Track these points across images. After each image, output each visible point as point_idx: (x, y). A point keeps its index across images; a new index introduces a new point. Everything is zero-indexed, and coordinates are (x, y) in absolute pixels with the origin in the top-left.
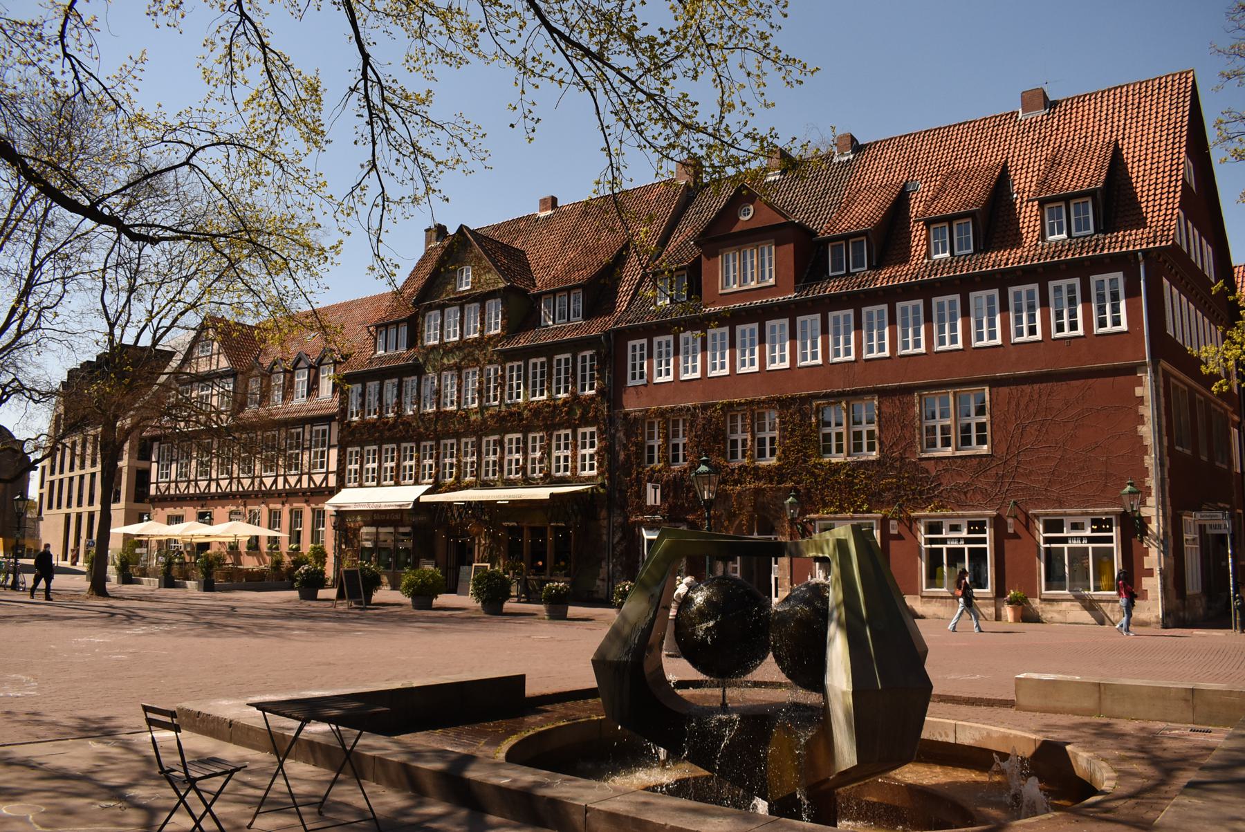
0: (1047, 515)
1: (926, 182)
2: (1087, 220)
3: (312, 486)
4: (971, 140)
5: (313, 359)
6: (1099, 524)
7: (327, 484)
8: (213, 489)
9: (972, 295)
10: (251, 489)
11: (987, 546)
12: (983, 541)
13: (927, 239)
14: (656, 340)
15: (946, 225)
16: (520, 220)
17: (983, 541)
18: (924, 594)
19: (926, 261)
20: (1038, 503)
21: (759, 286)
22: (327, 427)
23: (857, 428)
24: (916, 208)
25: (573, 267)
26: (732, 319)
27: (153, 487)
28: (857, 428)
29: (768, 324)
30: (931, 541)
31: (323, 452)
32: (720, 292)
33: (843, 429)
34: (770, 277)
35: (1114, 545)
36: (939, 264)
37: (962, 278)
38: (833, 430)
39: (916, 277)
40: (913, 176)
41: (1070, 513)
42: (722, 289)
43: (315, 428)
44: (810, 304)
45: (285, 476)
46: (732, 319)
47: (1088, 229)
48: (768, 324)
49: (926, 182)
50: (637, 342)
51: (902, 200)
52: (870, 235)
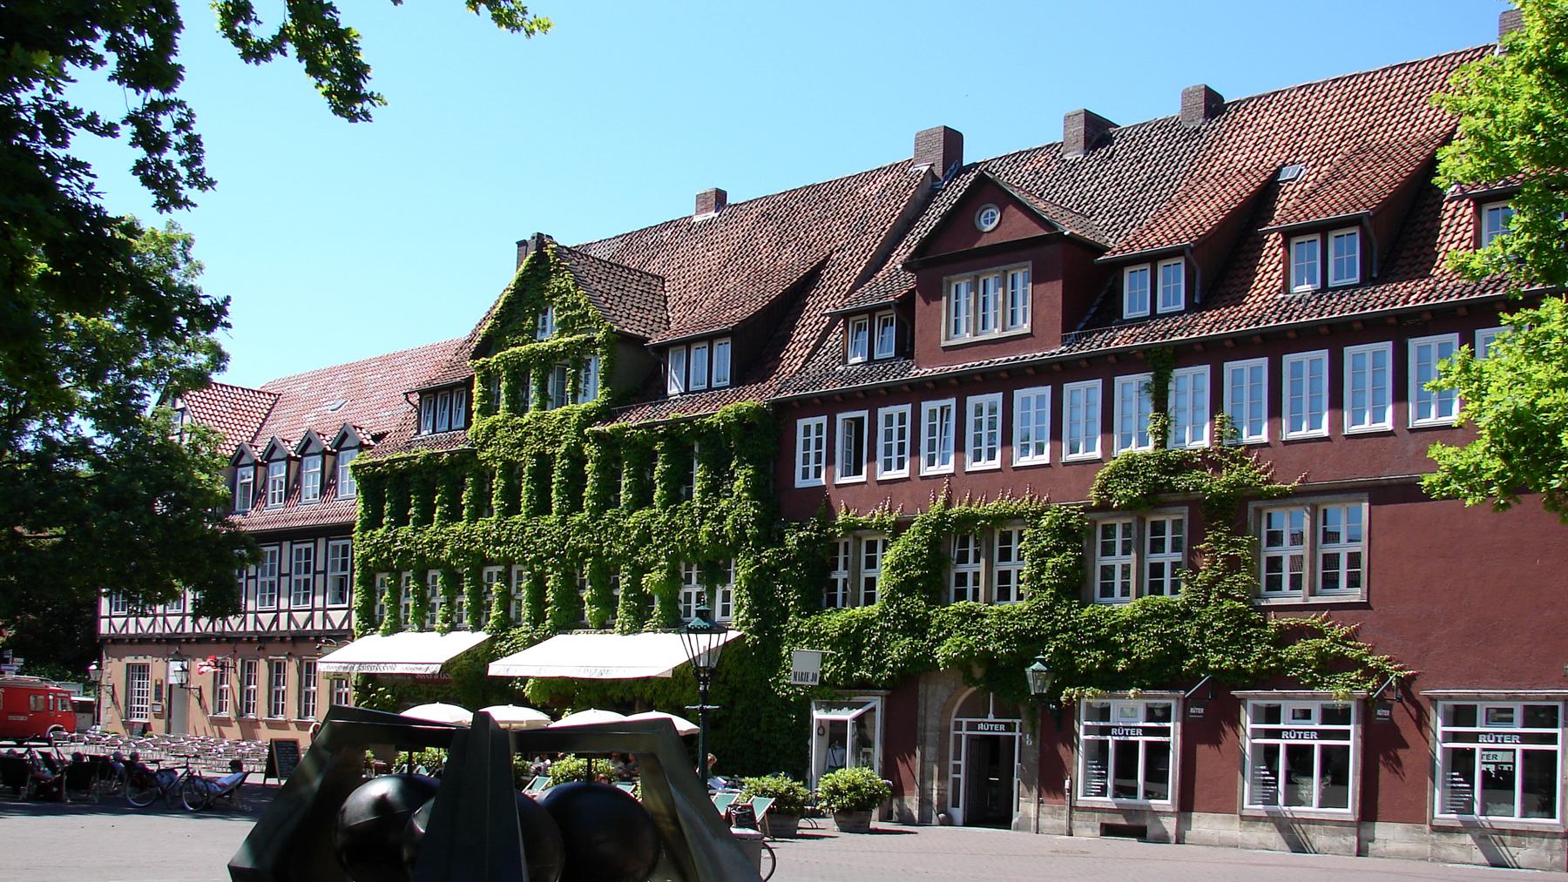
0: (1450, 698)
1: (1314, 166)
2: (1177, 289)
3: (329, 627)
4: (1405, 94)
5: (327, 443)
6: (1329, 715)
7: (127, 630)
8: (283, 626)
9: (1349, 351)
10: (346, 626)
11: (1350, 743)
12: (1345, 735)
13: (1286, 261)
14: (882, 412)
15: (1317, 237)
16: (666, 226)
17: (1345, 735)
18: (1245, 813)
19: (1281, 296)
20: (1443, 679)
21: (1006, 334)
22: (276, 548)
23: (1331, 549)
24: (1285, 208)
25: (727, 302)
26: (962, 385)
27: (104, 623)
28: (1331, 549)
29: (1018, 394)
30: (1456, 737)
31: (307, 581)
32: (944, 343)
33: (1303, 550)
34: (1025, 321)
35: (1350, 743)
36: (1299, 301)
37: (1332, 325)
38: (1286, 551)
39: (1257, 323)
40: (1297, 155)
41: (1486, 695)
42: (948, 339)
43: (296, 547)
44: (1084, 364)
45: (290, 611)
46: (962, 385)
47: (1177, 302)
48: (1018, 394)
49: (1314, 166)
50: (812, 422)
51: (1269, 190)
52: (1366, 223)
